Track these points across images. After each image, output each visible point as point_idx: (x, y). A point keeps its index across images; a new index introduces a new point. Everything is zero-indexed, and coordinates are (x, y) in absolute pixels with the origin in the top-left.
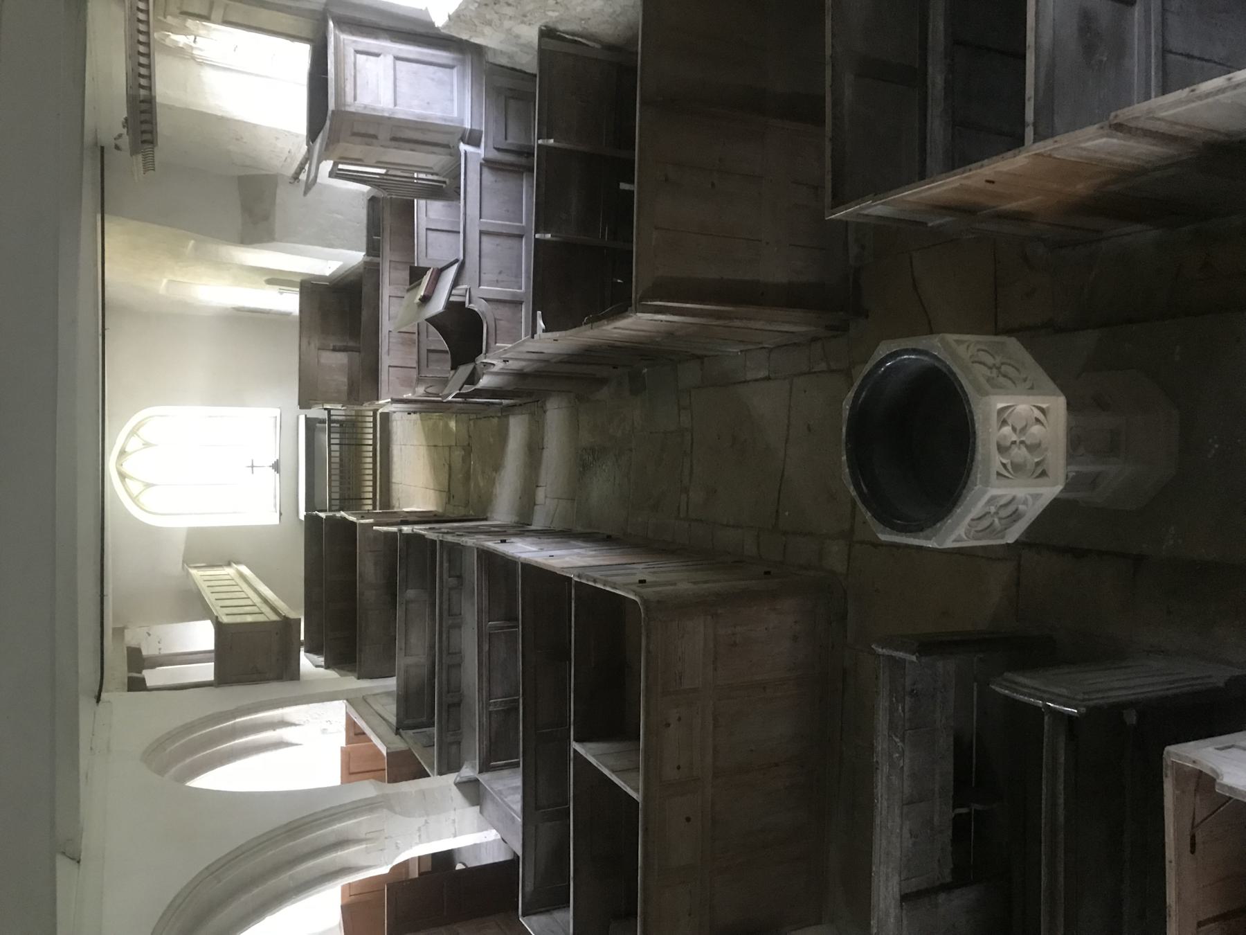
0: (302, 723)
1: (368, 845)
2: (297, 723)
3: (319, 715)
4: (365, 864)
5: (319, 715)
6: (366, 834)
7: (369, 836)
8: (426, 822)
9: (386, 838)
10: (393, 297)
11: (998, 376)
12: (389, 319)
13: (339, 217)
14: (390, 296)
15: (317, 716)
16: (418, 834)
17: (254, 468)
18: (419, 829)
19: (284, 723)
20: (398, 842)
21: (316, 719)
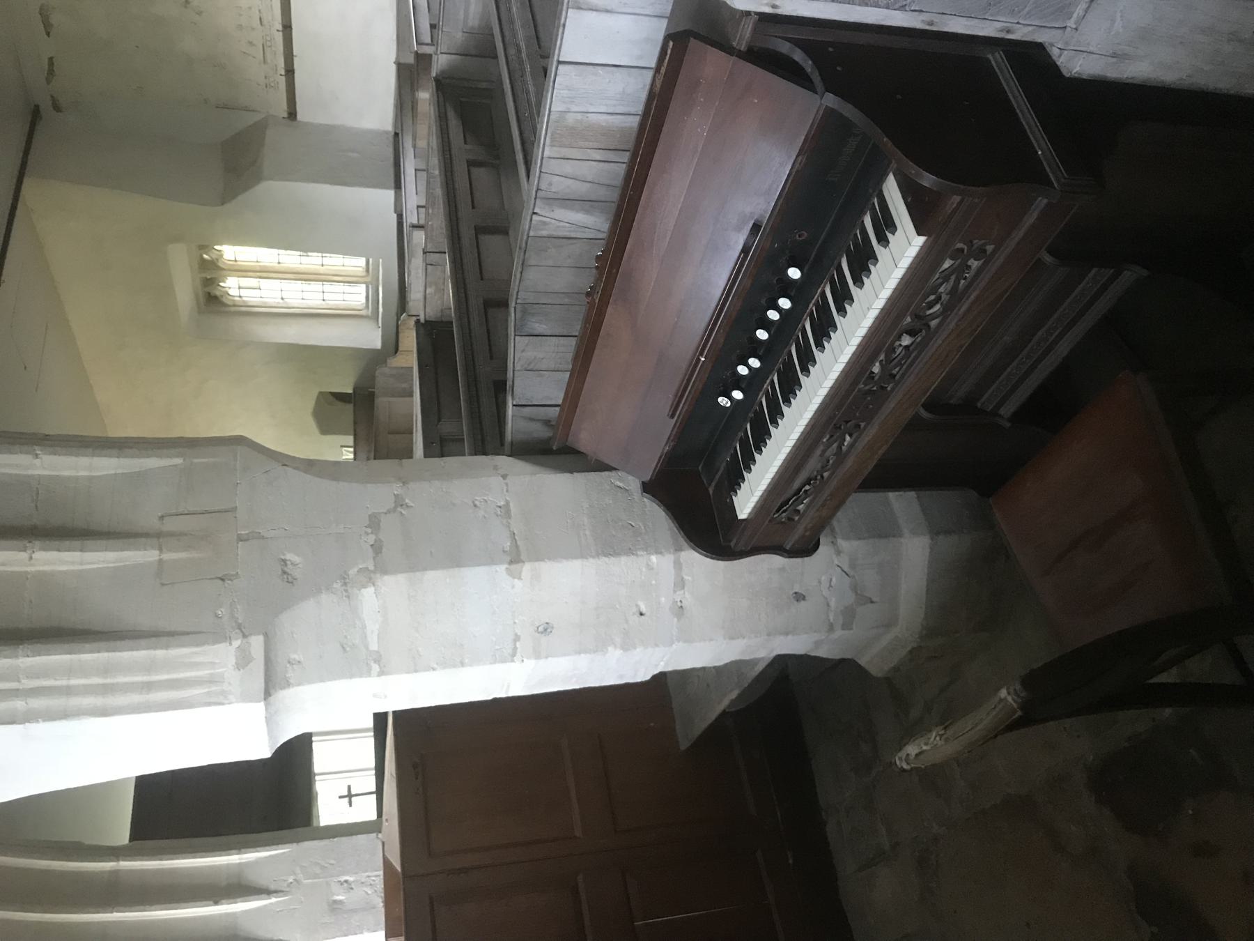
0: (283, 886)
1: (167, 556)
2: (272, 887)
3: (323, 868)
4: (145, 621)
5: (323, 868)
6: (162, 518)
7: (171, 525)
8: (399, 502)
9: (240, 539)
10: (419, 170)
11: (1154, 720)
12: (417, 194)
13: (355, 155)
14: (416, 170)
15: (318, 870)
16: (371, 539)
17: (354, 799)
18: (374, 523)
19: (238, 887)
20: (289, 556)
21: (316, 876)
